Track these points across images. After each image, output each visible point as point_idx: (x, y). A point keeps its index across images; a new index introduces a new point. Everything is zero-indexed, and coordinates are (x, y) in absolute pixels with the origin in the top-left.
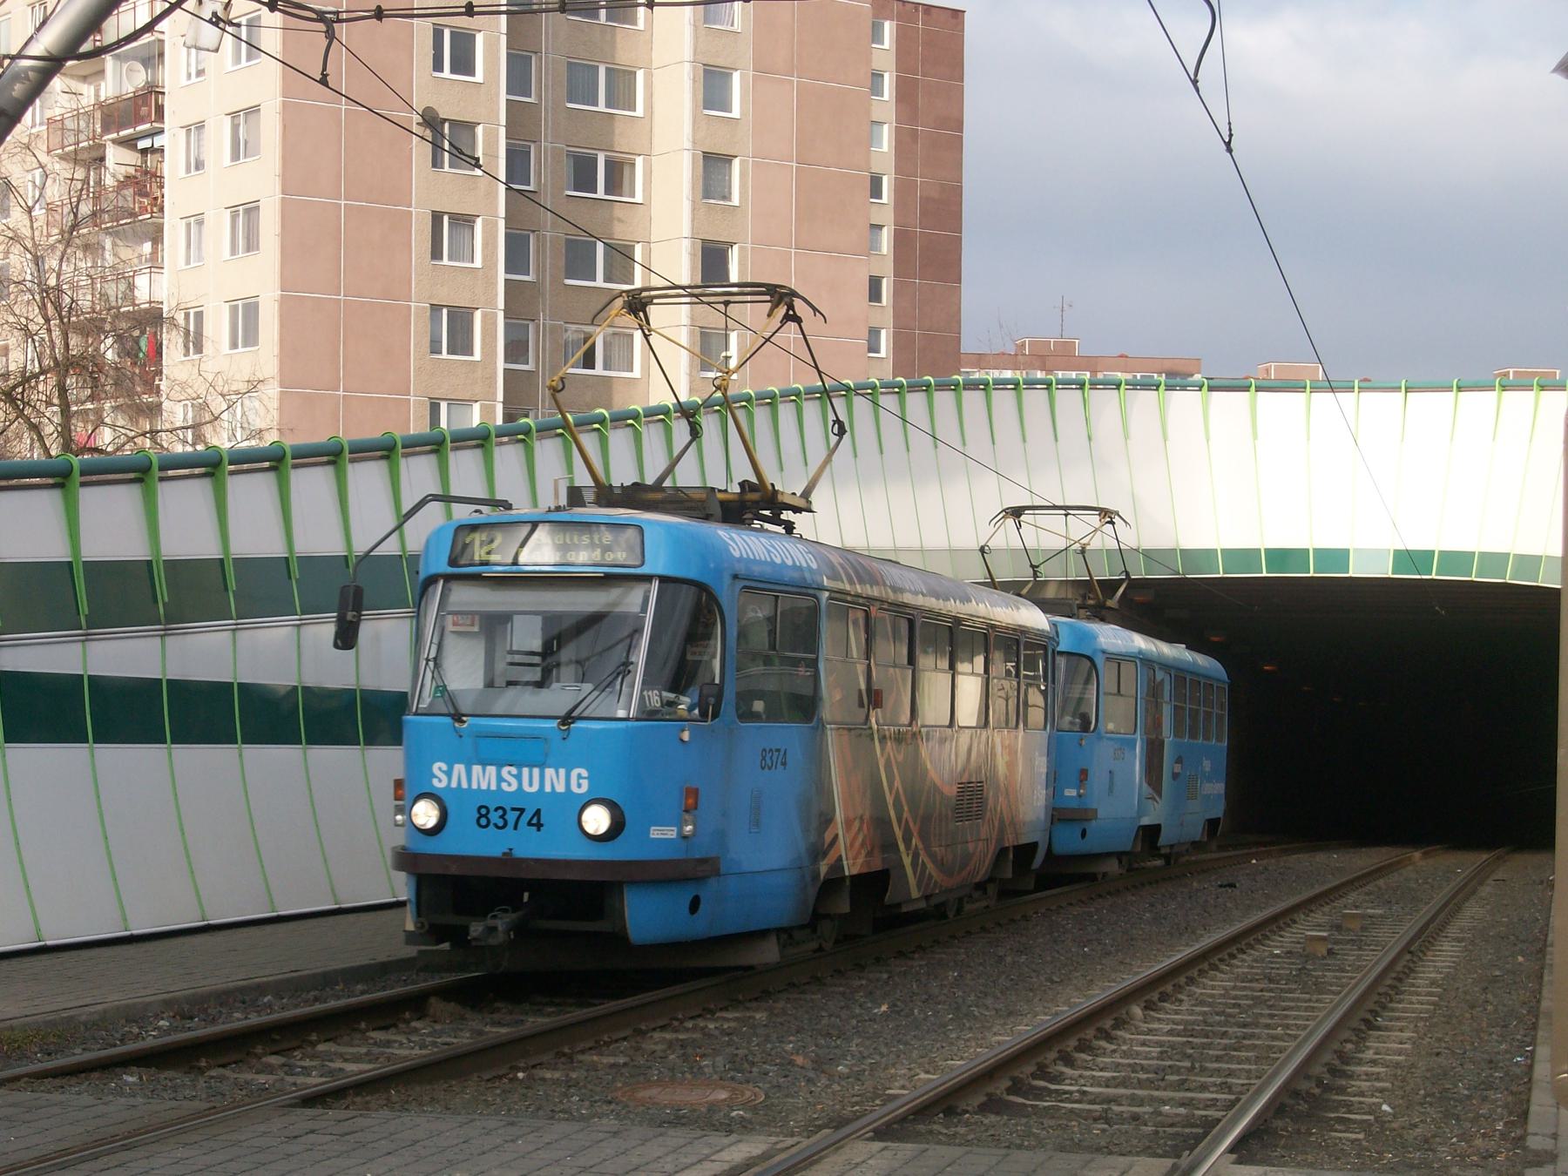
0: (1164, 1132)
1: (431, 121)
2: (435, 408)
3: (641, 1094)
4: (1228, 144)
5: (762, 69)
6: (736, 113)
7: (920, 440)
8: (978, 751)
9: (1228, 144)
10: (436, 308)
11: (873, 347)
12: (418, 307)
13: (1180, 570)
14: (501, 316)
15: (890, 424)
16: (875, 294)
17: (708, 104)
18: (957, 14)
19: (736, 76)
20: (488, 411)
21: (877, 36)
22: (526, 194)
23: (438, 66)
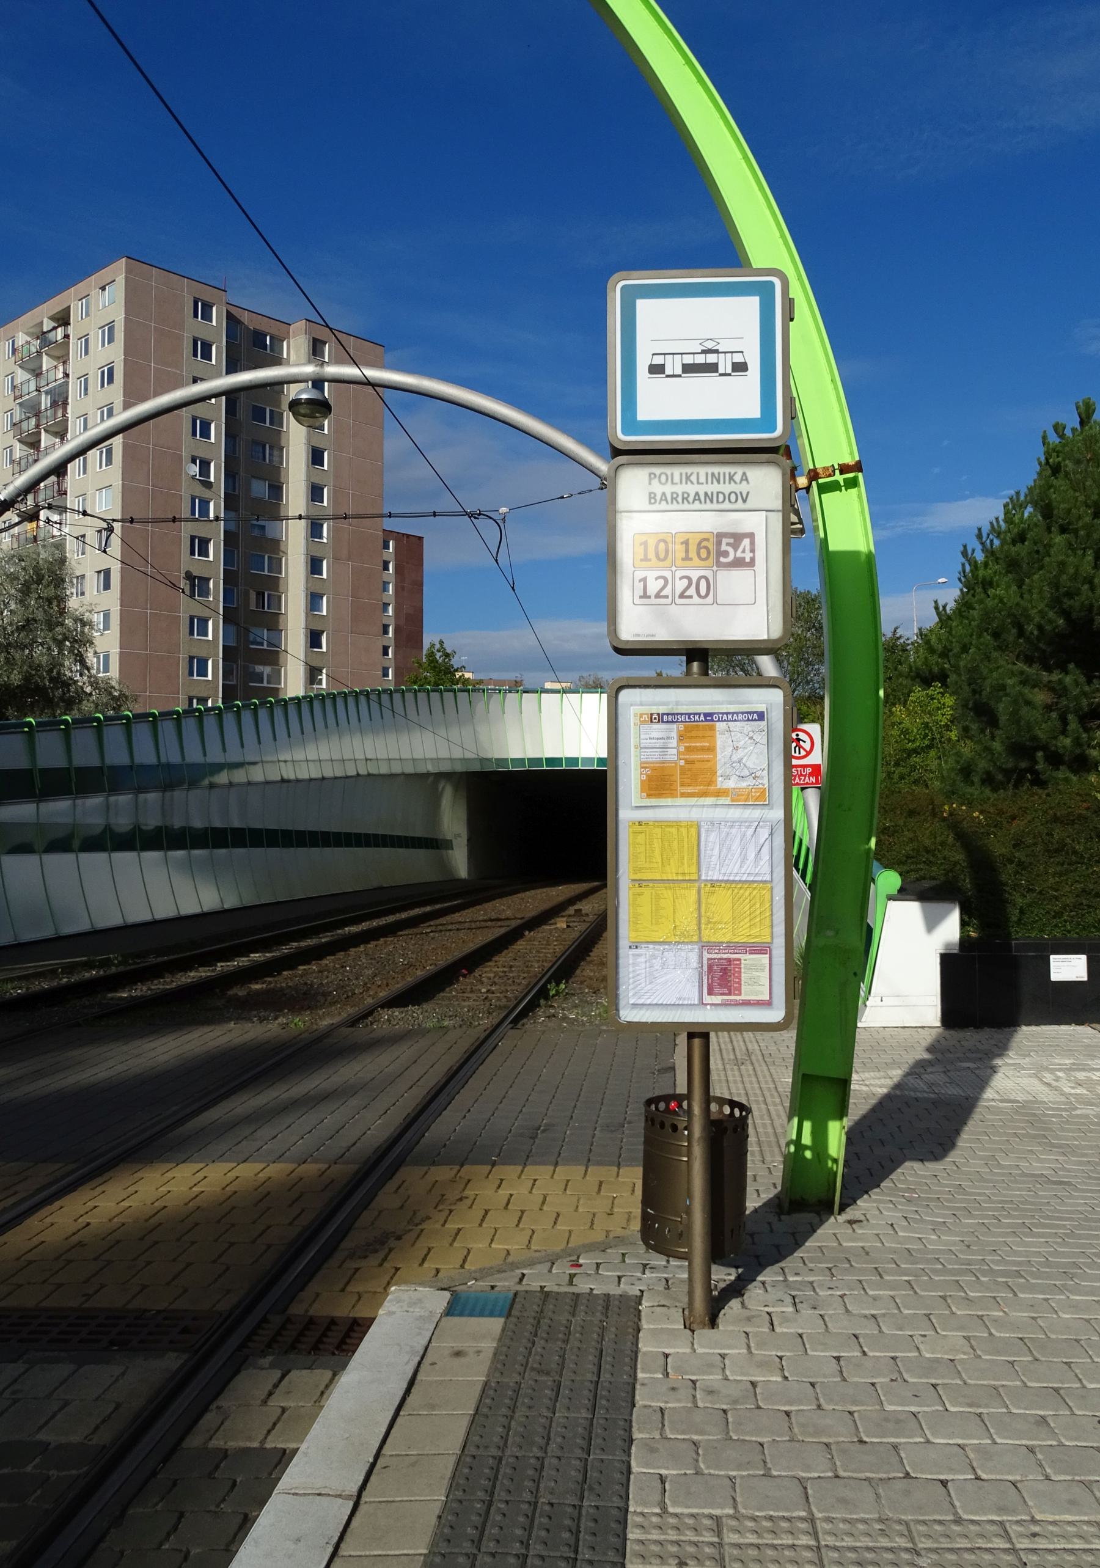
0: (835, 1309)
1: (189, 576)
2: (191, 700)
3: (230, 993)
4: (513, 588)
5: (336, 559)
6: (325, 576)
7: (387, 713)
8: (741, 1050)
9: (513, 588)
10: (191, 658)
11: (386, 674)
12: (183, 657)
13: (493, 768)
14: (221, 661)
15: (374, 706)
16: (386, 653)
17: (313, 573)
18: (420, 538)
19: (325, 563)
20: (215, 701)
21: (386, 547)
22: (578, 714)
23: (192, 553)
